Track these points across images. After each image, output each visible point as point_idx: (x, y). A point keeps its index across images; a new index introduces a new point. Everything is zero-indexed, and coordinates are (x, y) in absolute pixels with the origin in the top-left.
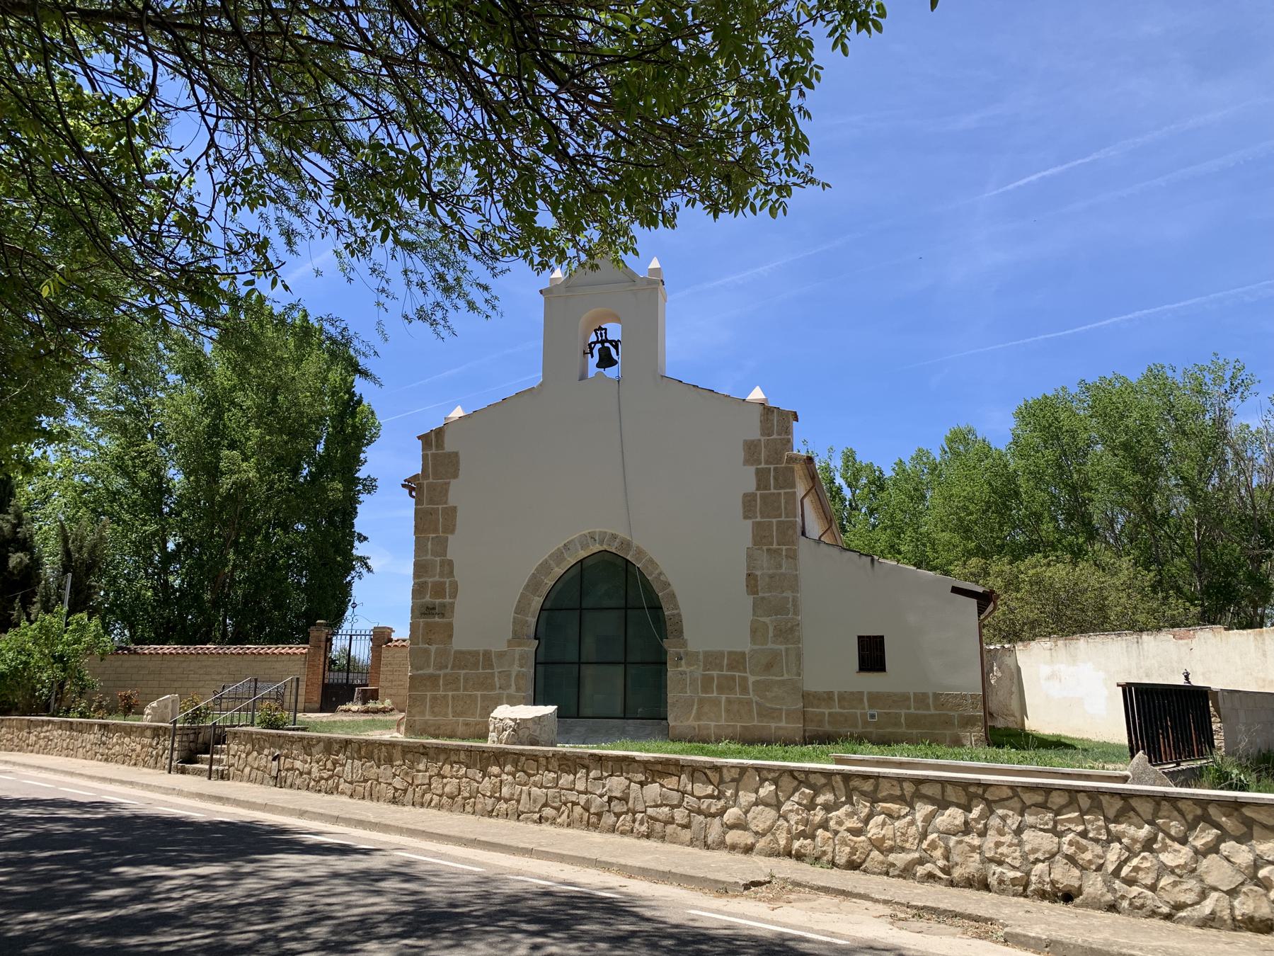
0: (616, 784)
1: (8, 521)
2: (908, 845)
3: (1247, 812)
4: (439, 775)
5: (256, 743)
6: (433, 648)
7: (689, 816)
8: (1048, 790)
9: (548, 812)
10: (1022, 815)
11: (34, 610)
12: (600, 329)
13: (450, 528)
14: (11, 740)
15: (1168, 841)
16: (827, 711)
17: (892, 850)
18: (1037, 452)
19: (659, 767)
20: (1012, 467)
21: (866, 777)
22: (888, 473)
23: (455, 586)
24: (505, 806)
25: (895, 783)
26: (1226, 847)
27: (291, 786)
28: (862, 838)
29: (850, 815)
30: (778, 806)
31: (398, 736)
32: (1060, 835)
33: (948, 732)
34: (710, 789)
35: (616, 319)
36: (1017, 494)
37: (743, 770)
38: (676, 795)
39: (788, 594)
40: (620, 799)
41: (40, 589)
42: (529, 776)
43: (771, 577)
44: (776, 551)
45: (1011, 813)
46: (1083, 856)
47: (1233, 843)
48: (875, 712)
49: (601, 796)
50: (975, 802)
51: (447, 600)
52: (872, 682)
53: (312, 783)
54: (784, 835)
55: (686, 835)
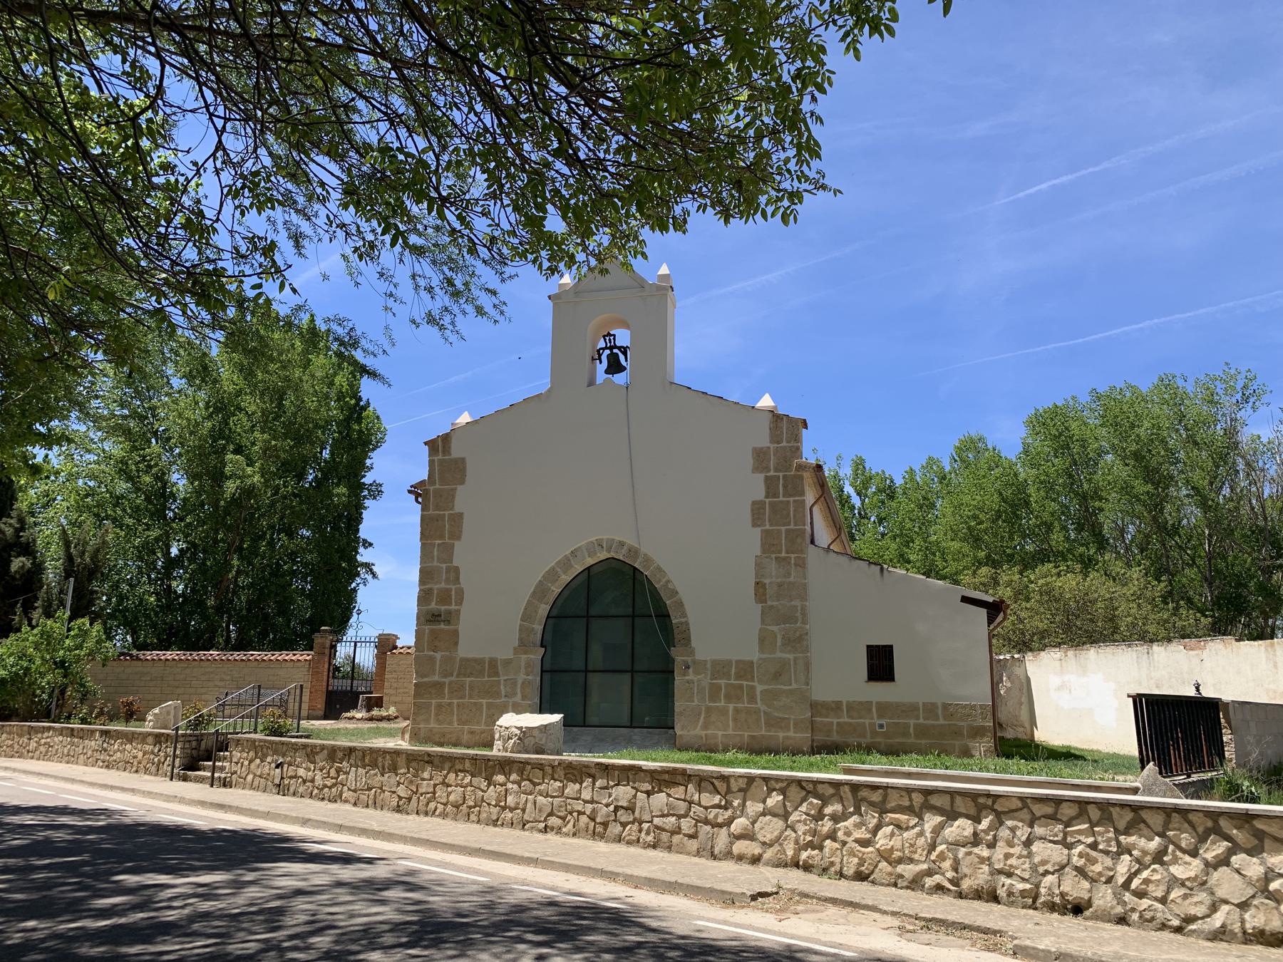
0: (623, 793)
1: (11, 525)
2: (916, 857)
3: (1258, 824)
4: (443, 783)
5: (259, 750)
6: (438, 656)
7: (696, 826)
8: (1058, 801)
9: (554, 821)
10: (1032, 827)
11: (35, 615)
12: (609, 334)
13: (456, 535)
14: (12, 746)
15: (1178, 853)
16: (835, 721)
17: (900, 861)
20: (1022, 476)
21: (874, 787)
22: (899, 482)
23: (460, 593)
24: (510, 815)
25: (904, 793)
26: (1237, 860)
27: (294, 794)
28: (870, 849)
29: (858, 826)
30: (786, 816)
32: (1069, 847)
33: (957, 743)
37: (751, 779)
38: (683, 805)
39: (797, 603)
40: (626, 809)
42: (535, 784)
43: (780, 585)
44: (784, 559)
45: (1020, 824)
46: (1093, 868)
47: (1244, 855)
49: (607, 805)
50: (984, 813)
51: (453, 607)
52: (880, 692)
53: (316, 791)
54: (792, 845)
55: (693, 845)
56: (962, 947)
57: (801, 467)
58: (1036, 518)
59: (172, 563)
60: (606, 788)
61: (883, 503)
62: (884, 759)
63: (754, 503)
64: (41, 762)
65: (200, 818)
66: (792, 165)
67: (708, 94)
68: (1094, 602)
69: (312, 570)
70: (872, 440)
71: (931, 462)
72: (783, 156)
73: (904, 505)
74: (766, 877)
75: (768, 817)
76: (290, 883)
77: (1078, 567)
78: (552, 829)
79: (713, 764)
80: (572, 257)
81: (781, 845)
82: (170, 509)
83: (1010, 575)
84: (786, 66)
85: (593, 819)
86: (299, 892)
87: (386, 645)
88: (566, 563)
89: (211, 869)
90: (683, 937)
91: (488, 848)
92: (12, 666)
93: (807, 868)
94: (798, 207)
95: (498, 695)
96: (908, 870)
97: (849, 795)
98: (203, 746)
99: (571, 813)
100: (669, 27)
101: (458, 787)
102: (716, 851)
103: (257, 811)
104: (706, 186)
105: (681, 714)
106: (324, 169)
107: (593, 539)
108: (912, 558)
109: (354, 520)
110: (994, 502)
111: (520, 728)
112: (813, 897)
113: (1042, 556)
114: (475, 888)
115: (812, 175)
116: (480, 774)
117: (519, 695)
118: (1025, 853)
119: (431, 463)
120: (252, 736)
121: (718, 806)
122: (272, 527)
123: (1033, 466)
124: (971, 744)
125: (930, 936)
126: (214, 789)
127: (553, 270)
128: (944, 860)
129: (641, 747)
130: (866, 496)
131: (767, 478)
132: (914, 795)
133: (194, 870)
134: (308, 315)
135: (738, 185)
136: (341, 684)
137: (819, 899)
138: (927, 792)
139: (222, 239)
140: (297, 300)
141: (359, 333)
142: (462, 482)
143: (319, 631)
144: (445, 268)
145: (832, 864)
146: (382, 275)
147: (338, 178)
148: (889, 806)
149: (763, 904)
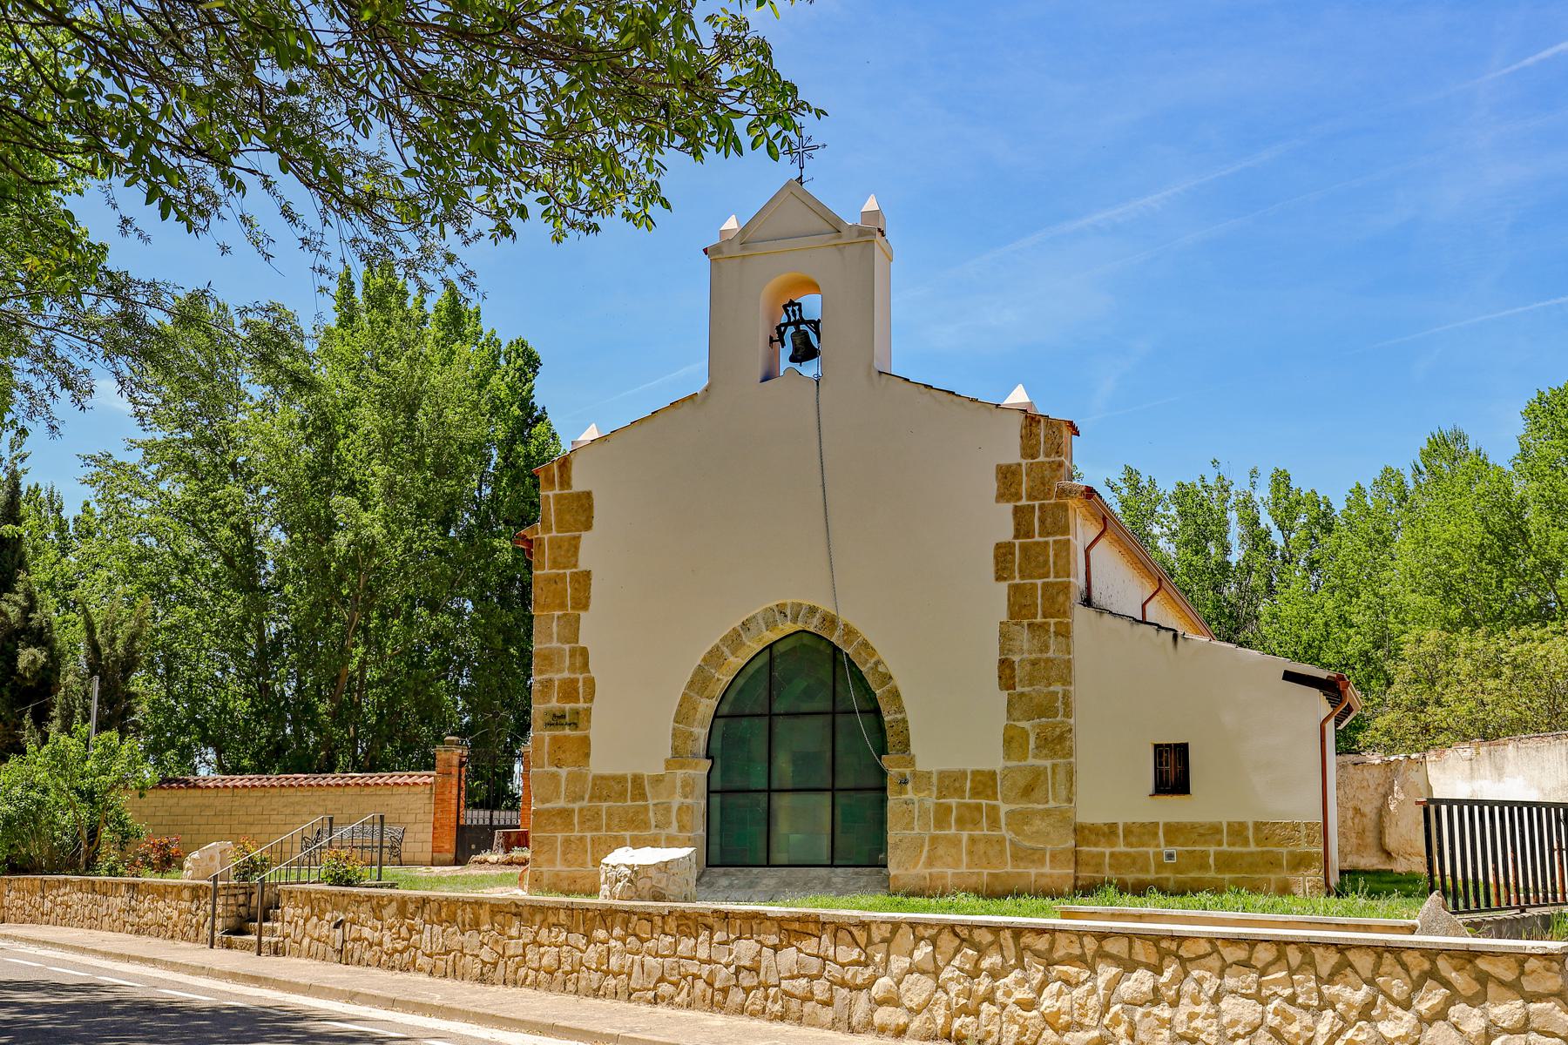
0: (745, 949)
1: (16, 603)
2: (1087, 1021)
3: (1482, 964)
4: (534, 942)
5: (316, 905)
6: (563, 772)
7: (831, 989)
8: (1252, 943)
9: (665, 988)
10: (1221, 977)
11: (53, 728)
12: (792, 303)
13: (582, 603)
14: (22, 908)
15: (1389, 1006)
16: (1108, 851)
17: (1068, 1028)
18: (1556, 469)
19: (796, 926)
20: (1518, 493)
21: (1040, 931)
22: (1339, 506)
23: (590, 684)
24: (614, 982)
25: (1074, 938)
26: (1455, 1012)
27: (359, 962)
28: (1034, 1013)
29: (1020, 983)
30: (936, 973)
31: (520, 894)
32: (1264, 1002)
33: (1272, 877)
34: (855, 953)
35: (813, 286)
36: (1525, 535)
37: (896, 926)
38: (817, 962)
39: (1057, 688)
40: (749, 970)
41: (59, 697)
42: (642, 941)
43: (1034, 663)
44: (1041, 626)
45: (1208, 974)
46: (1289, 1028)
47: (1463, 1005)
48: (1173, 850)
49: (727, 966)
50: (1167, 961)
51: (581, 705)
52: (1172, 809)
53: (384, 957)
54: (942, 1011)
55: (827, 1014)
59: (270, 651)
64: (58, 928)
71: (1388, 474)
85: (711, 985)
91: (563, 1023)
92: (20, 800)
95: (645, 825)
103: (297, 984)
105: (896, 846)
107: (772, 604)
108: (1355, 619)
110: (1475, 533)
111: (630, 867)
117: (675, 824)
121: (858, 963)
124: (1292, 878)
131: (1017, 510)
138: (1102, 936)
146: (305, 242)
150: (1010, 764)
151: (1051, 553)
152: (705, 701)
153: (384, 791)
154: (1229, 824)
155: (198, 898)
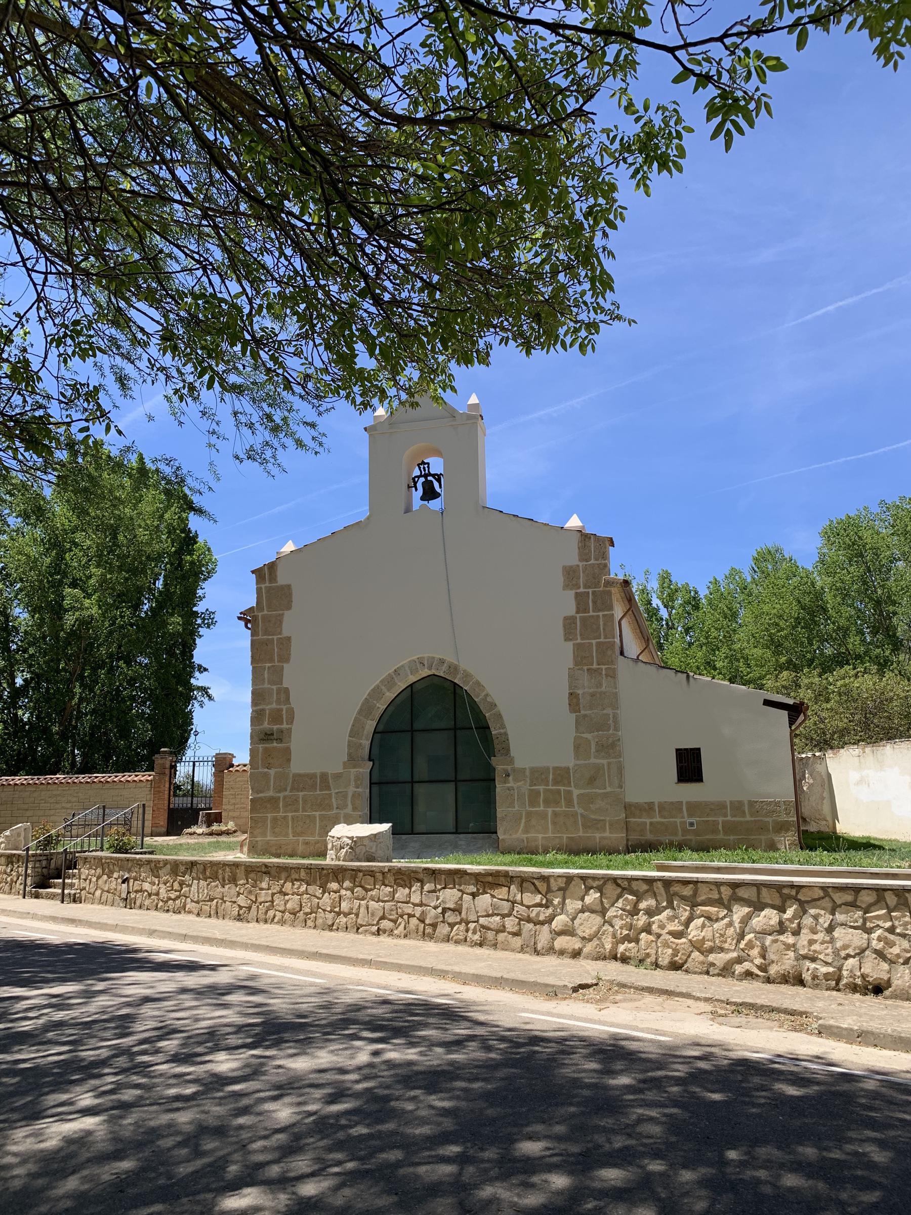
0: (450, 896)
2: (726, 946)
5: (106, 867)
6: (272, 772)
7: (519, 924)
8: (857, 889)
9: (386, 924)
12: (423, 463)
16: (648, 821)
17: (711, 950)
19: (490, 879)
20: (819, 584)
22: (703, 593)
24: (345, 920)
25: (713, 887)
27: (140, 907)
28: (683, 940)
29: (671, 919)
30: (603, 912)
32: (869, 931)
33: (763, 837)
34: (538, 898)
35: (438, 453)
36: (825, 610)
37: (569, 879)
39: (609, 711)
40: (453, 910)
42: (367, 890)
43: (592, 695)
44: (596, 670)
45: (822, 912)
46: (891, 950)
49: (435, 908)
50: (788, 903)
51: (285, 726)
52: (690, 792)
53: (161, 904)
54: (610, 939)
55: (517, 942)
56: (771, 1028)
57: (609, 583)
58: (834, 623)
59: (17, 693)
60: (434, 891)
61: (689, 614)
62: (695, 855)
63: (566, 618)
65: (52, 932)
66: (588, 298)
67: (504, 232)
68: (891, 700)
69: (150, 695)
70: (675, 554)
71: (734, 573)
72: (579, 289)
73: (708, 617)
74: (587, 970)
75: (587, 914)
76: (138, 991)
77: (874, 668)
78: (385, 931)
79: (534, 866)
80: (383, 392)
81: (599, 939)
82: (13, 642)
83: (811, 678)
84: (578, 204)
85: (423, 921)
86: (147, 1000)
87: (223, 764)
88: (389, 682)
89: (63, 980)
90: (510, 1030)
91: (325, 951)
93: (625, 960)
94: (595, 337)
95: (330, 807)
96: (719, 959)
97: (662, 890)
98: (53, 865)
99: (402, 916)
100: (466, 169)
101: (296, 895)
102: (539, 947)
103: (106, 924)
104: (507, 320)
105: (503, 819)
106: (145, 317)
107: (415, 658)
109: (188, 647)
111: (351, 838)
112: (631, 987)
113: (841, 660)
114: (313, 989)
115: (607, 306)
116: (314, 883)
117: (350, 806)
118: (827, 938)
119: (259, 591)
120: (99, 854)
121: (539, 905)
122: (111, 656)
123: (828, 574)
124: (776, 839)
125: (741, 1019)
126: (65, 905)
127: (366, 405)
128: (752, 948)
129: (466, 852)
130: (673, 608)
131: (577, 595)
132: (723, 889)
133: (47, 981)
134: (136, 455)
135: (537, 318)
136: (181, 802)
137: (636, 988)
138: (735, 885)
139: (47, 384)
140: (122, 442)
141: (185, 471)
142: (289, 607)
143: (159, 752)
144: (264, 405)
145: (648, 955)
146: (204, 413)
147: (158, 322)
148: (699, 899)
149: (584, 995)
150: (578, 762)
151: (601, 623)
152: (369, 722)
153: (120, 786)
154: (731, 802)
155: (12, 863)
